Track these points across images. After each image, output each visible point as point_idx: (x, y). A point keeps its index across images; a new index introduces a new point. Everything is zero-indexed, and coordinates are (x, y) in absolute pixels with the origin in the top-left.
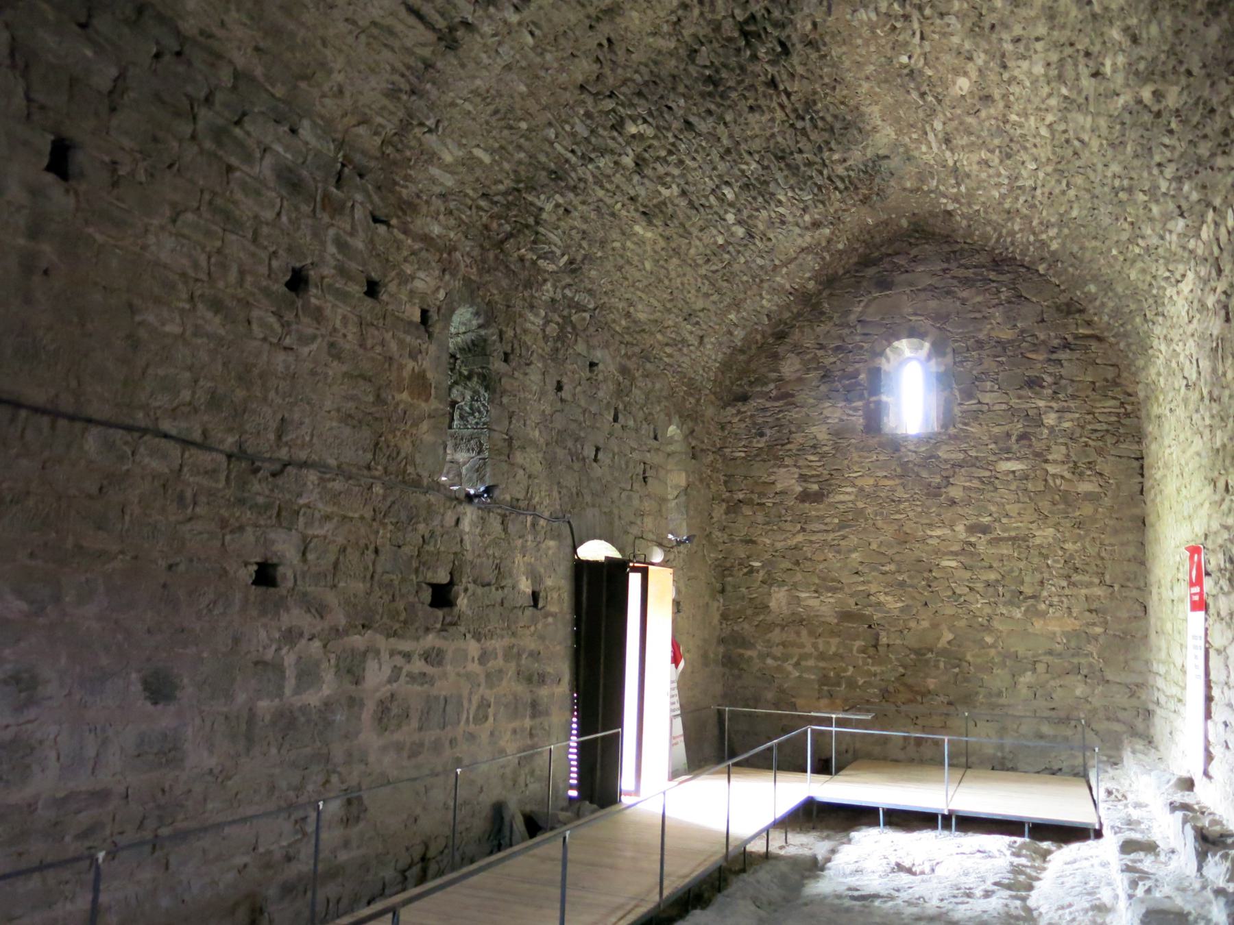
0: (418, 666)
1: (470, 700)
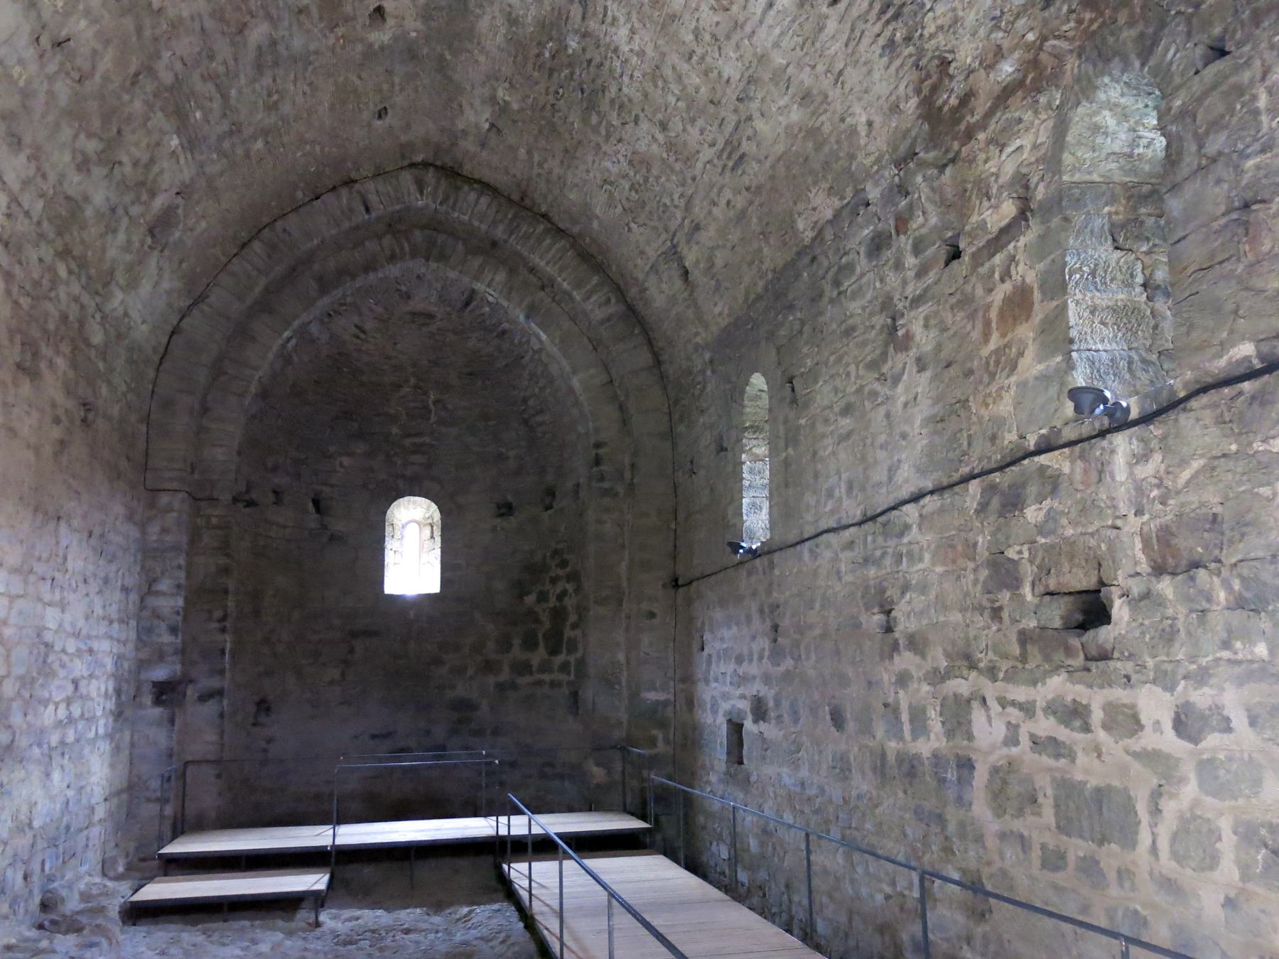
0: (1046, 726)
1: (1156, 811)
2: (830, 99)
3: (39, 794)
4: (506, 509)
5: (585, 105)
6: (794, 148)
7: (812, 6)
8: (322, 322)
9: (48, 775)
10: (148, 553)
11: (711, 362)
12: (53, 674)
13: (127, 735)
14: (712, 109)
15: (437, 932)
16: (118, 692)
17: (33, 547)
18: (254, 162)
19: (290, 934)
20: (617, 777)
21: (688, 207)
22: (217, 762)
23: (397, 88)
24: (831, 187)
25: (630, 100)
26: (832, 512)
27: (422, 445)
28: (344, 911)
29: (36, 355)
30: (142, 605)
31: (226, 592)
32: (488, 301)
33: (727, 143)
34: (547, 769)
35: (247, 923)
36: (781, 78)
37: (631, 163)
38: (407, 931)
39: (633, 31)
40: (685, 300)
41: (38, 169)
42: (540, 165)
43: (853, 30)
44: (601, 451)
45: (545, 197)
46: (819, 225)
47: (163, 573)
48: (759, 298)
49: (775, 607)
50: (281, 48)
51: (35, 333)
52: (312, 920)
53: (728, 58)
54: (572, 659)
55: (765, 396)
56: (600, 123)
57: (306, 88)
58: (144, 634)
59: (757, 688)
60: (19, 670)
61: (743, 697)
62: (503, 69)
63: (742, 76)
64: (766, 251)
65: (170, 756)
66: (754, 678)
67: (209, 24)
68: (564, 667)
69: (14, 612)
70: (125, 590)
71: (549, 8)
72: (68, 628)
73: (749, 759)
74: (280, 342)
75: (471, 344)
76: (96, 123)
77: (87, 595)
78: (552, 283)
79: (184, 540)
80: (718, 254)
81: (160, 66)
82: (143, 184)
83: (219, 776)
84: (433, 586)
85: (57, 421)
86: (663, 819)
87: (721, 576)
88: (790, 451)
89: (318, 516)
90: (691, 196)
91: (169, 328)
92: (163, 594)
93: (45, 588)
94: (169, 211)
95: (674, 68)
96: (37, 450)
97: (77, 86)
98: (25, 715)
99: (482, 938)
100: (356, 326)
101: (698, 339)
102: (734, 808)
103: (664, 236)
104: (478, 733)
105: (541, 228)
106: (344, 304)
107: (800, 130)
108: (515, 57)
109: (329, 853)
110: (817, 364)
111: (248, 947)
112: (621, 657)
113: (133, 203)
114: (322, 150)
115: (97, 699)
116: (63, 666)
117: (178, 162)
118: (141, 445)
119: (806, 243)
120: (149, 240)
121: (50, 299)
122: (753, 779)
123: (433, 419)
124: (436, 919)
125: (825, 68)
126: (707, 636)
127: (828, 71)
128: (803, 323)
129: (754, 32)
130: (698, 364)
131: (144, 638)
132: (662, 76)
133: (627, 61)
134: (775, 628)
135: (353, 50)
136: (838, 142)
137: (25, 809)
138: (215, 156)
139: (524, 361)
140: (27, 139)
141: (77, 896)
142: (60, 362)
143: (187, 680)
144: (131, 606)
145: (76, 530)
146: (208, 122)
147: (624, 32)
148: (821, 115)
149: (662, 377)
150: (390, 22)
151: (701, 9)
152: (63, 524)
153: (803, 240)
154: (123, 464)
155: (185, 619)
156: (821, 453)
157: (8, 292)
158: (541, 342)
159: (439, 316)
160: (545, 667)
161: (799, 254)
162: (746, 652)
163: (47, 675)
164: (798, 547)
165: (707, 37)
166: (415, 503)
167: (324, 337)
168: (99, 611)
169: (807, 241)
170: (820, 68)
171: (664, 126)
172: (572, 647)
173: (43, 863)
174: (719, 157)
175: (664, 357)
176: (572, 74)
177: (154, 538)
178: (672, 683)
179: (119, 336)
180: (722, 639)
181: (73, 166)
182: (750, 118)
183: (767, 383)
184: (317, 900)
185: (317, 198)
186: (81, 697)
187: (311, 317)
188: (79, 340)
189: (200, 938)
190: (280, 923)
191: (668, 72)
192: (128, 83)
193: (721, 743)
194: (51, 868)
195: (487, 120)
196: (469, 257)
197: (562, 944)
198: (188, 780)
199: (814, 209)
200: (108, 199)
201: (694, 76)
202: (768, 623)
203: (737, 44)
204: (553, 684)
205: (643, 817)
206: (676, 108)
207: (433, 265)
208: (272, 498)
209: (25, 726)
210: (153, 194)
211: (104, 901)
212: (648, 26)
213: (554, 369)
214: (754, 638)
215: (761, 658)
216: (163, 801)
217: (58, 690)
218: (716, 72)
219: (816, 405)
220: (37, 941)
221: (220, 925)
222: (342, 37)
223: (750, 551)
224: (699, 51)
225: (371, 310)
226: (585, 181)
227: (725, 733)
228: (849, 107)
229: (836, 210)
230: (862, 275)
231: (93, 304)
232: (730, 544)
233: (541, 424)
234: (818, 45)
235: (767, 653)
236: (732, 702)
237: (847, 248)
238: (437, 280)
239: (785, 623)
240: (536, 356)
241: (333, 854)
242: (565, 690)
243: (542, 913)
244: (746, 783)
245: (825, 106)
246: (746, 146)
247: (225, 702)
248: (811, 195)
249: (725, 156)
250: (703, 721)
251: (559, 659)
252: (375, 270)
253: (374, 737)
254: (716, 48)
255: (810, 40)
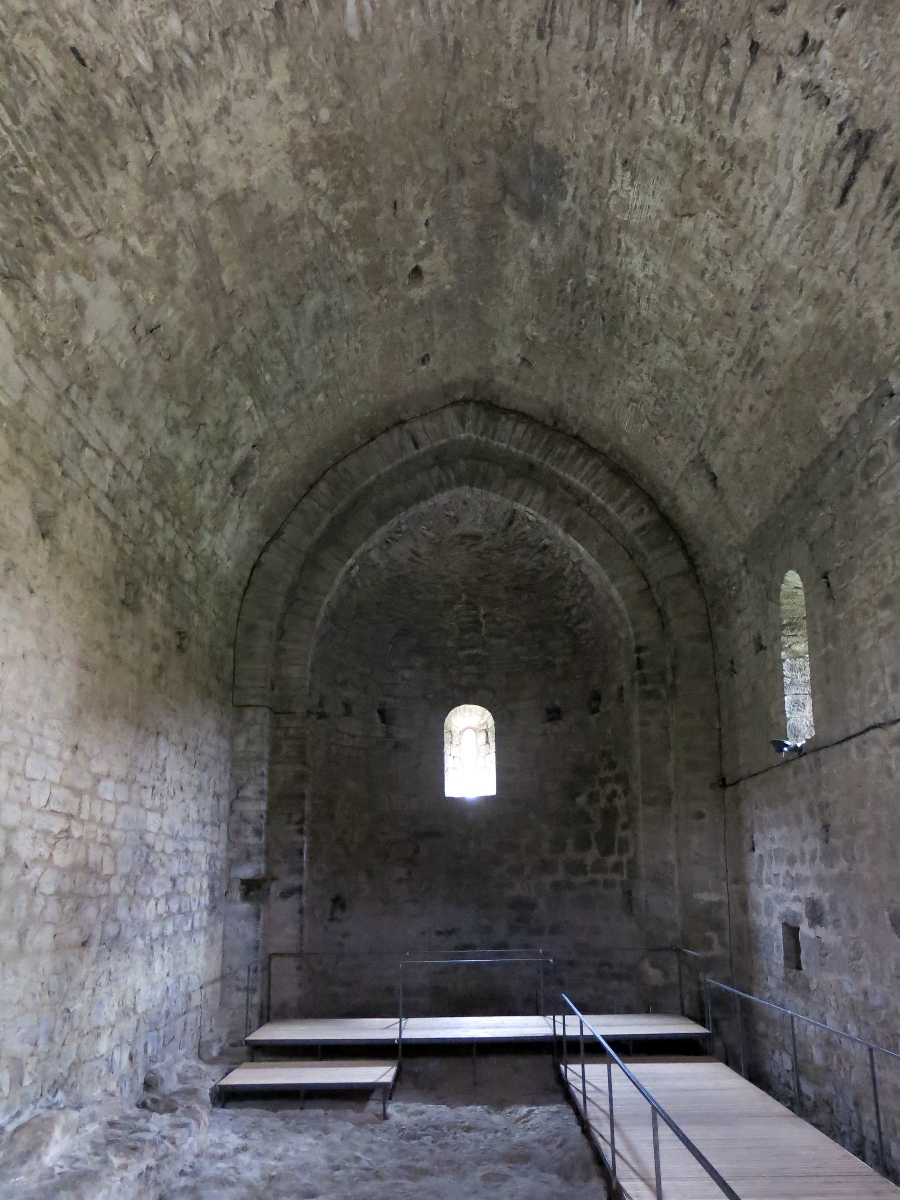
2: (844, 297)
3: (142, 983)
4: (554, 715)
5: (607, 331)
6: (812, 349)
7: (819, 211)
8: (381, 548)
9: (150, 964)
10: (237, 762)
11: (745, 563)
12: (154, 872)
13: (221, 926)
14: (727, 321)
15: (497, 1132)
16: (212, 889)
17: (137, 759)
18: (317, 413)
19: (360, 1125)
20: (674, 979)
21: (712, 418)
22: (299, 955)
23: (437, 336)
24: (854, 382)
25: (649, 322)
26: (879, 707)
27: (476, 655)
28: (408, 1105)
29: (137, 593)
30: (232, 811)
31: (303, 797)
32: (529, 521)
33: (746, 351)
34: (606, 969)
35: (321, 1112)
36: (793, 283)
37: (654, 380)
38: (469, 1130)
39: (646, 258)
40: (715, 505)
41: (138, 435)
42: (570, 390)
43: (862, 228)
44: (643, 655)
45: (576, 419)
46: (844, 421)
47: (248, 780)
48: (789, 497)
49: (826, 806)
50: (335, 314)
51: (138, 574)
52: (380, 1113)
53: (740, 271)
54: (625, 859)
55: (801, 593)
56: (622, 347)
57: (359, 346)
58: (234, 835)
59: (811, 891)
60: (124, 869)
61: (797, 899)
62: (530, 308)
63: (755, 287)
64: (792, 450)
65: (257, 948)
66: (807, 879)
67: (273, 300)
68: (617, 868)
69: (120, 818)
70: (217, 796)
71: (567, 248)
72: (166, 830)
73: (807, 964)
74: (344, 570)
75: (516, 560)
76: (184, 393)
77: (184, 801)
78: (587, 498)
79: (266, 750)
80: (744, 457)
81: (234, 339)
82: (224, 440)
83: (299, 968)
84: (451, 791)
85: (156, 649)
86: (724, 1025)
87: (768, 774)
88: (830, 647)
89: (383, 725)
90: (715, 405)
91: (251, 564)
92: (249, 799)
93: (147, 795)
94: (247, 462)
95: (688, 287)
96: (140, 674)
97: (168, 364)
98: (130, 909)
99: (539, 1141)
100: (412, 551)
101: (731, 542)
102: (792, 1017)
103: (690, 446)
104: (539, 932)
105: (574, 449)
106: (399, 533)
107: (817, 330)
108: (540, 295)
109: (397, 1046)
110: (852, 558)
111: (321, 1136)
112: (672, 857)
113: (217, 458)
114: (375, 399)
115: (193, 896)
116: (163, 866)
117: (253, 420)
118: (229, 668)
119: (832, 440)
120: (231, 488)
121: (149, 544)
122: (813, 986)
123: (484, 631)
124: (497, 1118)
125: (837, 268)
126: (757, 836)
127: (841, 270)
128: (834, 517)
129: (763, 244)
130: (732, 565)
131: (234, 840)
132: (677, 296)
133: (643, 286)
134: (826, 827)
135: (397, 307)
136: (856, 337)
137: (130, 994)
138: (283, 412)
139: (566, 574)
140: (128, 412)
141: (176, 1078)
142: (159, 598)
143: (271, 878)
144: (222, 809)
145: (174, 744)
146: (277, 383)
147: (638, 260)
148: (837, 313)
149: (698, 581)
150: (427, 279)
151: (710, 230)
152: (162, 738)
153: (829, 436)
154: (213, 683)
155: (268, 823)
156: (862, 648)
157: (115, 541)
158: (580, 555)
159: (485, 537)
160: (599, 868)
161: (826, 450)
162: (798, 854)
163: (148, 874)
164: (845, 744)
165: (718, 255)
166: (470, 711)
167: (383, 563)
168: (194, 816)
169: (833, 438)
170: (832, 269)
171: (683, 343)
172: (624, 847)
173: (146, 1045)
174: (738, 366)
175: (699, 561)
176: (593, 305)
177: (242, 748)
178: (725, 884)
179: (208, 573)
180: (773, 840)
181: (166, 431)
182: (766, 325)
183: (802, 580)
184: (387, 1092)
185: (373, 440)
186: (179, 893)
187: (372, 545)
188: (174, 580)
189: (279, 1124)
190: (351, 1114)
191: (683, 292)
192: (209, 356)
193: (778, 947)
194: (153, 1051)
195: (519, 355)
196: (510, 481)
197: (614, 1152)
198: (273, 971)
199: (837, 405)
200: (195, 456)
201: (708, 292)
202: (819, 825)
203: (748, 257)
204: (607, 884)
205: (702, 1022)
206: (693, 324)
207: (477, 491)
208: (341, 710)
209: (130, 920)
210: (233, 450)
211: (197, 1084)
212: (660, 251)
213: (594, 579)
214: (805, 838)
215: (813, 859)
216: (250, 990)
217: (159, 887)
218: (729, 285)
219: (853, 600)
220: (137, 1119)
221: (298, 1112)
222: (386, 297)
223: (795, 749)
224: (711, 268)
225: (424, 535)
226: (613, 402)
227: (781, 937)
228: (866, 302)
229: (860, 404)
230: (892, 465)
231: (185, 546)
232: (774, 742)
233: (585, 632)
234: (828, 247)
235: (819, 854)
236: (787, 905)
237: (875, 440)
238: (481, 504)
239: (837, 823)
240: (576, 569)
241: (400, 1047)
242: (619, 891)
243: (597, 1119)
244: (806, 990)
245: (841, 305)
246: (764, 352)
247: (304, 899)
248: (834, 392)
249: (744, 363)
250: (758, 923)
251: (613, 859)
252: (426, 499)
253: (439, 933)
254: (728, 264)
255: (818, 244)
